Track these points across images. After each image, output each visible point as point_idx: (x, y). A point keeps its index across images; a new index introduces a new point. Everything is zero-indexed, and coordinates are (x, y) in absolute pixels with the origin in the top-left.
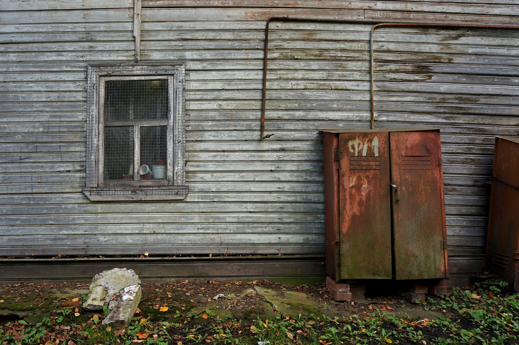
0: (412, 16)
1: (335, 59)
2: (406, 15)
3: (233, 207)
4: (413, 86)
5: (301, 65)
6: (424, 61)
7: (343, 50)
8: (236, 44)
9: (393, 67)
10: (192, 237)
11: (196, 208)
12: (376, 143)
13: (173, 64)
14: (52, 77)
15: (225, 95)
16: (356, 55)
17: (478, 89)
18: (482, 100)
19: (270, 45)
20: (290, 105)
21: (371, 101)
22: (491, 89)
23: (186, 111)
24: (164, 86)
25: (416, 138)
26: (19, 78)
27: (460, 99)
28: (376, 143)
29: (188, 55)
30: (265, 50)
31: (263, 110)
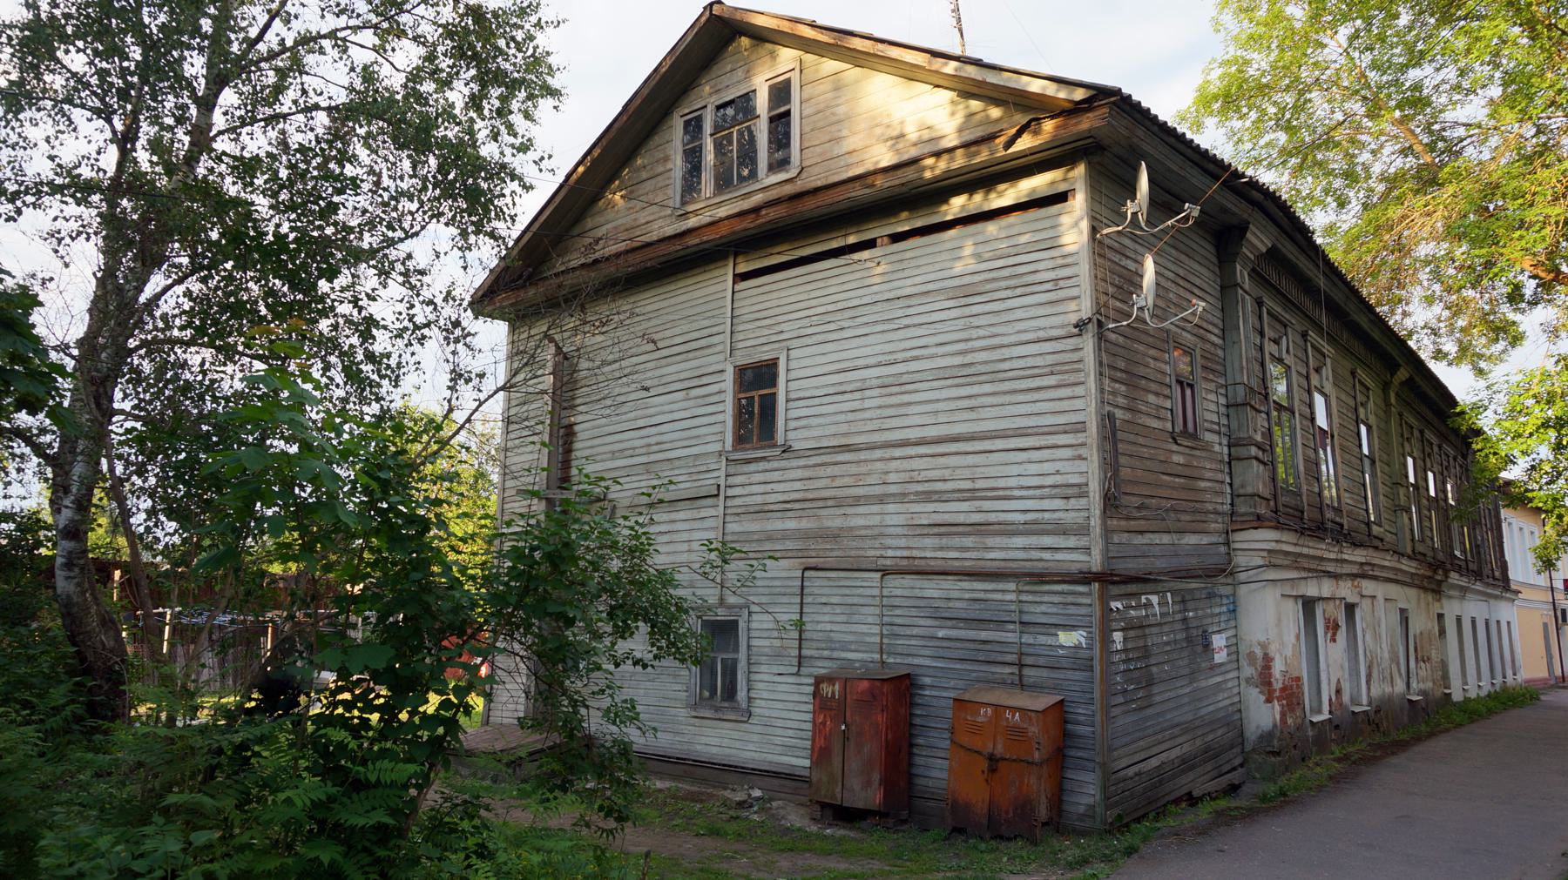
0: (916, 562)
3: (779, 732)
10: (753, 754)
12: (837, 687)
13: (741, 607)
21: (882, 643)
23: (749, 646)
24: (736, 622)
25: (865, 685)
28: (837, 687)
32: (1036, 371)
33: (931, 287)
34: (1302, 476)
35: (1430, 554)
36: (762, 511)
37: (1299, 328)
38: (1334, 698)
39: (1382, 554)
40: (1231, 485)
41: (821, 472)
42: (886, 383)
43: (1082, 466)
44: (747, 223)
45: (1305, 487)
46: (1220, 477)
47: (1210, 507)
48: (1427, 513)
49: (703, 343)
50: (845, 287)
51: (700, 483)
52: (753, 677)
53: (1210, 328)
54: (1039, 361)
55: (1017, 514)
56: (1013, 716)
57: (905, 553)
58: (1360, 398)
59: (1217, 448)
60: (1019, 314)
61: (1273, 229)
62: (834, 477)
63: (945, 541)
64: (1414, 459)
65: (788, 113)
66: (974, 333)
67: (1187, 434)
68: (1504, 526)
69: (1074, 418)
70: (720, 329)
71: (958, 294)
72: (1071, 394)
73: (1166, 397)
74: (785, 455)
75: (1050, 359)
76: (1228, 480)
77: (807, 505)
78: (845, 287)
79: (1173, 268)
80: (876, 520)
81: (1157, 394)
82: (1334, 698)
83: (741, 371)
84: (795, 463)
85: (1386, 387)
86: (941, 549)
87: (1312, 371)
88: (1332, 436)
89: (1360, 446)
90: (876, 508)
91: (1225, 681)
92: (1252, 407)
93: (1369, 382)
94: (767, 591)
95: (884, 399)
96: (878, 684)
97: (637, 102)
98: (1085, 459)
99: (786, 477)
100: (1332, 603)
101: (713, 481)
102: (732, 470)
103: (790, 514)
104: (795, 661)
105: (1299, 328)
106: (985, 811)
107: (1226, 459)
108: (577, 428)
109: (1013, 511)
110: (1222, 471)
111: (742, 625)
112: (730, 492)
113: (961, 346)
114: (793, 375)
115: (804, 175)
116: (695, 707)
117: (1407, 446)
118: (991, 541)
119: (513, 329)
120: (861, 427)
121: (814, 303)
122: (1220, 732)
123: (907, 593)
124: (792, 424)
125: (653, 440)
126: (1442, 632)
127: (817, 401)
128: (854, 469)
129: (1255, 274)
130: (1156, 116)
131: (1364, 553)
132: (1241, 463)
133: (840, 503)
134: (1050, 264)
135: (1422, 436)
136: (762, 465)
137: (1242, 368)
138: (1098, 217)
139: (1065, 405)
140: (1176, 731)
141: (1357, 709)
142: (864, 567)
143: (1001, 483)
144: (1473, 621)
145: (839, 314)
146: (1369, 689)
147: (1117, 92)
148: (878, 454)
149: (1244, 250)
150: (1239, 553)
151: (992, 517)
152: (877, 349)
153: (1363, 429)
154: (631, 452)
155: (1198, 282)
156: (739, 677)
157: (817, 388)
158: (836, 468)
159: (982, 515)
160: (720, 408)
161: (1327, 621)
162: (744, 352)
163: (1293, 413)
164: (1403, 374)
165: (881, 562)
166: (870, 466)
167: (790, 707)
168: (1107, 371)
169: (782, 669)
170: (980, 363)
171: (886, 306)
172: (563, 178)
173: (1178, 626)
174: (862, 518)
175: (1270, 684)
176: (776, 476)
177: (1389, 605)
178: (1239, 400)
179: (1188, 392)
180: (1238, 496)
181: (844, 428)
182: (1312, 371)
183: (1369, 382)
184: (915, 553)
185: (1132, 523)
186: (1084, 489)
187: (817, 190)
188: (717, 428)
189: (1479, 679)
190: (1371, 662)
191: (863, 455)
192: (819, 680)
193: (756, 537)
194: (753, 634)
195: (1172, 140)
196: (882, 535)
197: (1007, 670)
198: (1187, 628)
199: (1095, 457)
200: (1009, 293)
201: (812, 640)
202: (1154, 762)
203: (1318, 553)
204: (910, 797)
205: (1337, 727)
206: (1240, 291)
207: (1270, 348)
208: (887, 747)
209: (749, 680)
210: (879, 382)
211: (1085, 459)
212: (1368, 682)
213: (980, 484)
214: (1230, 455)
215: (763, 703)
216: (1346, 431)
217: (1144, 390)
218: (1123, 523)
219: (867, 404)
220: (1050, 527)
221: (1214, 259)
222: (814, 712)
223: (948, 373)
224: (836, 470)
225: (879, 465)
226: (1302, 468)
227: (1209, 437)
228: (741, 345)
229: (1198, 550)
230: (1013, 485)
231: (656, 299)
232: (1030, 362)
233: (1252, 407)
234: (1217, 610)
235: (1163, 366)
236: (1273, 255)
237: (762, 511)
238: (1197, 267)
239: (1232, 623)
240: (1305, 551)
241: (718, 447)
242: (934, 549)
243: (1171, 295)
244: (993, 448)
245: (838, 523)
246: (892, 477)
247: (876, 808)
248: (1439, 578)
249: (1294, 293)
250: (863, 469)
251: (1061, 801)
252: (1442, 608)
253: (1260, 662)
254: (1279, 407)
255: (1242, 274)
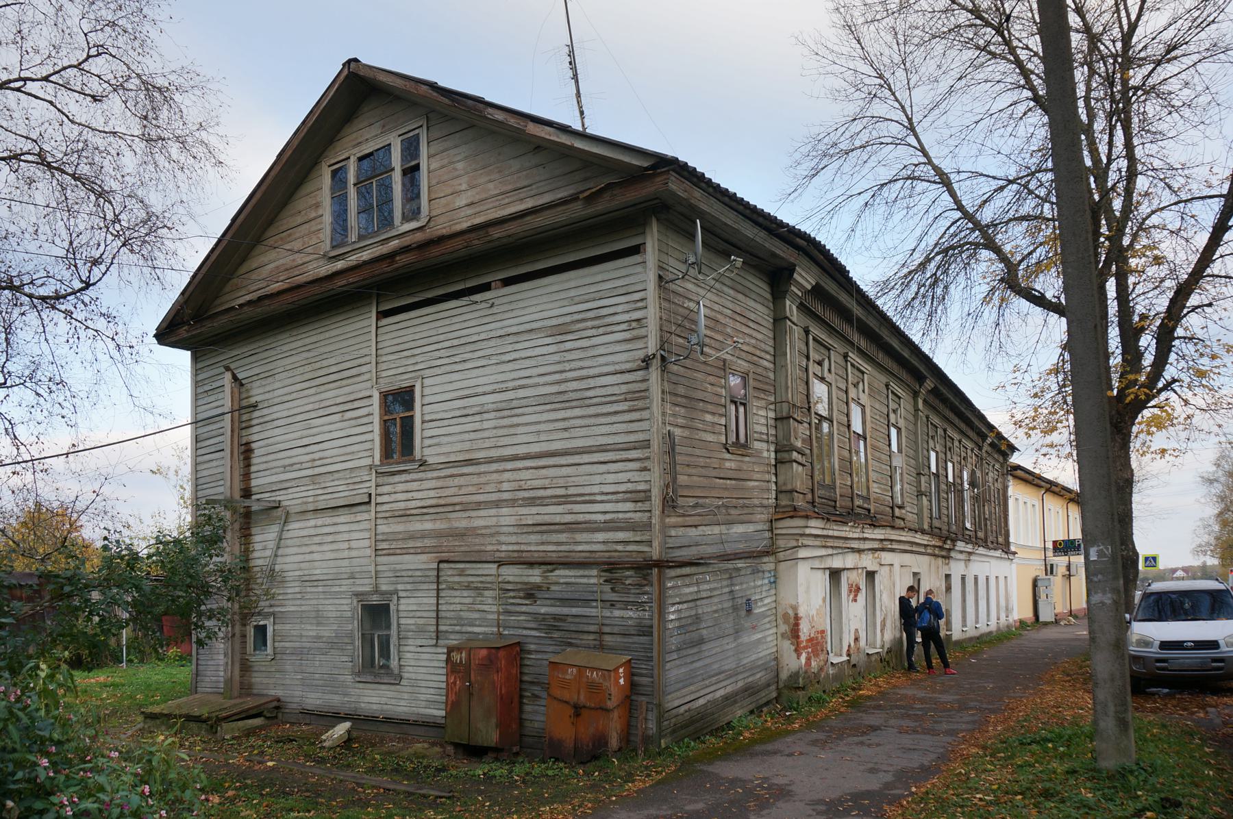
0: (524, 555)
1: (477, 588)
2: (520, 554)
3: (423, 690)
4: (524, 609)
5: (457, 593)
6: (531, 589)
7: (482, 582)
8: (423, 579)
9: (512, 594)
10: (405, 709)
11: (405, 689)
12: (463, 655)
14: (337, 601)
15: (419, 614)
16: (489, 585)
17: (566, 611)
18: (570, 620)
19: (441, 579)
20: (452, 622)
22: (574, 611)
23: (399, 624)
25: (484, 652)
26: (323, 602)
27: (555, 618)
28: (463, 655)
29: (400, 587)
30: (438, 583)
31: (437, 625)
32: (614, 398)
33: (534, 325)
34: (837, 473)
35: (945, 528)
36: (405, 515)
37: (842, 351)
38: (852, 644)
39: (898, 532)
40: (776, 483)
41: (450, 482)
42: (500, 407)
43: (645, 476)
44: (385, 267)
45: (838, 482)
46: (767, 477)
47: (756, 502)
48: (945, 496)
49: (354, 372)
50: (466, 324)
51: (355, 492)
52: (402, 648)
53: (763, 355)
54: (616, 390)
55: (599, 515)
56: (592, 674)
57: (516, 548)
58: (892, 405)
59: (765, 454)
60: (602, 350)
61: (815, 269)
62: (460, 487)
63: (545, 537)
64: (937, 453)
65: (418, 165)
66: (567, 366)
67: (740, 447)
68: (1011, 502)
69: (641, 437)
70: (367, 359)
71: (554, 332)
72: (639, 417)
73: (721, 415)
74: (422, 468)
75: (624, 388)
76: (774, 479)
77: (441, 510)
78: (466, 324)
79: (730, 305)
80: (492, 521)
81: (713, 414)
82: (852, 644)
83: (385, 396)
84: (429, 475)
85: (915, 394)
86: (543, 543)
87: (851, 387)
88: (865, 439)
89: (890, 445)
90: (493, 512)
91: (765, 637)
92: (794, 419)
93: (900, 392)
94: (411, 580)
95: (499, 421)
96: (493, 651)
97: (289, 153)
98: (649, 470)
99: (423, 487)
100: (855, 572)
101: (365, 490)
102: (380, 480)
103: (427, 517)
104: (434, 635)
105: (842, 351)
106: (572, 745)
107: (773, 462)
108: (254, 446)
109: (596, 512)
110: (769, 472)
111: (392, 607)
112: (380, 500)
113: (557, 377)
114: (427, 400)
115: (432, 224)
116: (359, 674)
117: (931, 442)
118: (580, 537)
119: (195, 359)
120: (481, 444)
121: (442, 338)
122: (758, 676)
123: (517, 579)
124: (427, 442)
125: (316, 456)
126: (948, 589)
127: (446, 423)
128: (475, 480)
129: (802, 307)
130: (710, 180)
131: (883, 532)
132: (783, 466)
133: (465, 507)
134: (626, 307)
135: (945, 433)
136: (404, 477)
137: (787, 388)
138: (665, 266)
139: (635, 426)
140: (721, 677)
141: (871, 651)
142: (484, 559)
143: (587, 490)
144: (976, 578)
145: (462, 348)
146: (883, 635)
147: (674, 161)
148: (494, 467)
149: (793, 288)
150: (778, 537)
151: (581, 518)
152: (492, 379)
153: (894, 432)
154: (298, 466)
155: (753, 316)
156: (579, 609)
157: (446, 411)
158: (462, 479)
159: (573, 516)
160: (369, 428)
161: (851, 586)
162: (387, 380)
163: (832, 422)
164: (929, 384)
165: (498, 554)
166: (489, 477)
167: (432, 670)
168: (668, 397)
169: (424, 642)
170: (572, 391)
171: (499, 341)
172: (228, 222)
173: (726, 597)
174: (483, 519)
175: (798, 637)
176: (415, 486)
177: (904, 569)
178: (784, 414)
179: (741, 409)
180: (781, 492)
181: (467, 446)
182: (851, 387)
183: (900, 392)
184: (523, 548)
185: (687, 518)
186: (648, 494)
187: (442, 239)
188: (367, 446)
189: (977, 622)
190: (886, 615)
191: (483, 468)
192: (450, 650)
193: (401, 536)
194: (401, 614)
195: (726, 199)
196: (498, 533)
197: (592, 637)
198: (733, 599)
199: (656, 468)
200: (594, 332)
201: (446, 618)
202: (702, 702)
203: (843, 534)
204: (522, 735)
205: (854, 666)
206: (789, 323)
207: (816, 369)
208: (502, 698)
209: (399, 652)
210: (494, 406)
211: (649, 470)
212: (882, 630)
213: (572, 491)
214: (776, 459)
215: (410, 669)
216: (878, 433)
217: (702, 411)
218: (680, 519)
219: (486, 425)
220: (622, 525)
221: (769, 296)
222: (447, 675)
223: (547, 400)
224: (462, 481)
225: (495, 476)
226: (837, 466)
227: (757, 445)
228: (384, 374)
229: (746, 537)
230: (597, 491)
231: (314, 332)
232: (609, 391)
233: (794, 419)
234: (759, 583)
235: (719, 389)
236: (817, 291)
237: (405, 515)
238: (752, 303)
239: (773, 592)
240: (831, 533)
241: (368, 461)
242: (537, 544)
243: (729, 330)
244: (582, 462)
245: (464, 524)
246: (505, 486)
247: (493, 745)
248: (947, 547)
249: (836, 322)
250: (483, 479)
251: (629, 734)
252: (950, 569)
253: (792, 621)
254: (821, 418)
255: (791, 308)
